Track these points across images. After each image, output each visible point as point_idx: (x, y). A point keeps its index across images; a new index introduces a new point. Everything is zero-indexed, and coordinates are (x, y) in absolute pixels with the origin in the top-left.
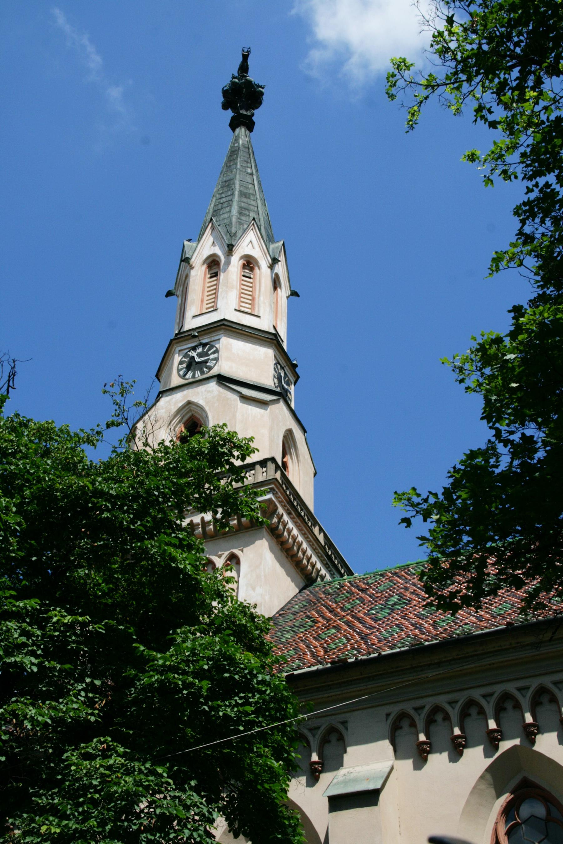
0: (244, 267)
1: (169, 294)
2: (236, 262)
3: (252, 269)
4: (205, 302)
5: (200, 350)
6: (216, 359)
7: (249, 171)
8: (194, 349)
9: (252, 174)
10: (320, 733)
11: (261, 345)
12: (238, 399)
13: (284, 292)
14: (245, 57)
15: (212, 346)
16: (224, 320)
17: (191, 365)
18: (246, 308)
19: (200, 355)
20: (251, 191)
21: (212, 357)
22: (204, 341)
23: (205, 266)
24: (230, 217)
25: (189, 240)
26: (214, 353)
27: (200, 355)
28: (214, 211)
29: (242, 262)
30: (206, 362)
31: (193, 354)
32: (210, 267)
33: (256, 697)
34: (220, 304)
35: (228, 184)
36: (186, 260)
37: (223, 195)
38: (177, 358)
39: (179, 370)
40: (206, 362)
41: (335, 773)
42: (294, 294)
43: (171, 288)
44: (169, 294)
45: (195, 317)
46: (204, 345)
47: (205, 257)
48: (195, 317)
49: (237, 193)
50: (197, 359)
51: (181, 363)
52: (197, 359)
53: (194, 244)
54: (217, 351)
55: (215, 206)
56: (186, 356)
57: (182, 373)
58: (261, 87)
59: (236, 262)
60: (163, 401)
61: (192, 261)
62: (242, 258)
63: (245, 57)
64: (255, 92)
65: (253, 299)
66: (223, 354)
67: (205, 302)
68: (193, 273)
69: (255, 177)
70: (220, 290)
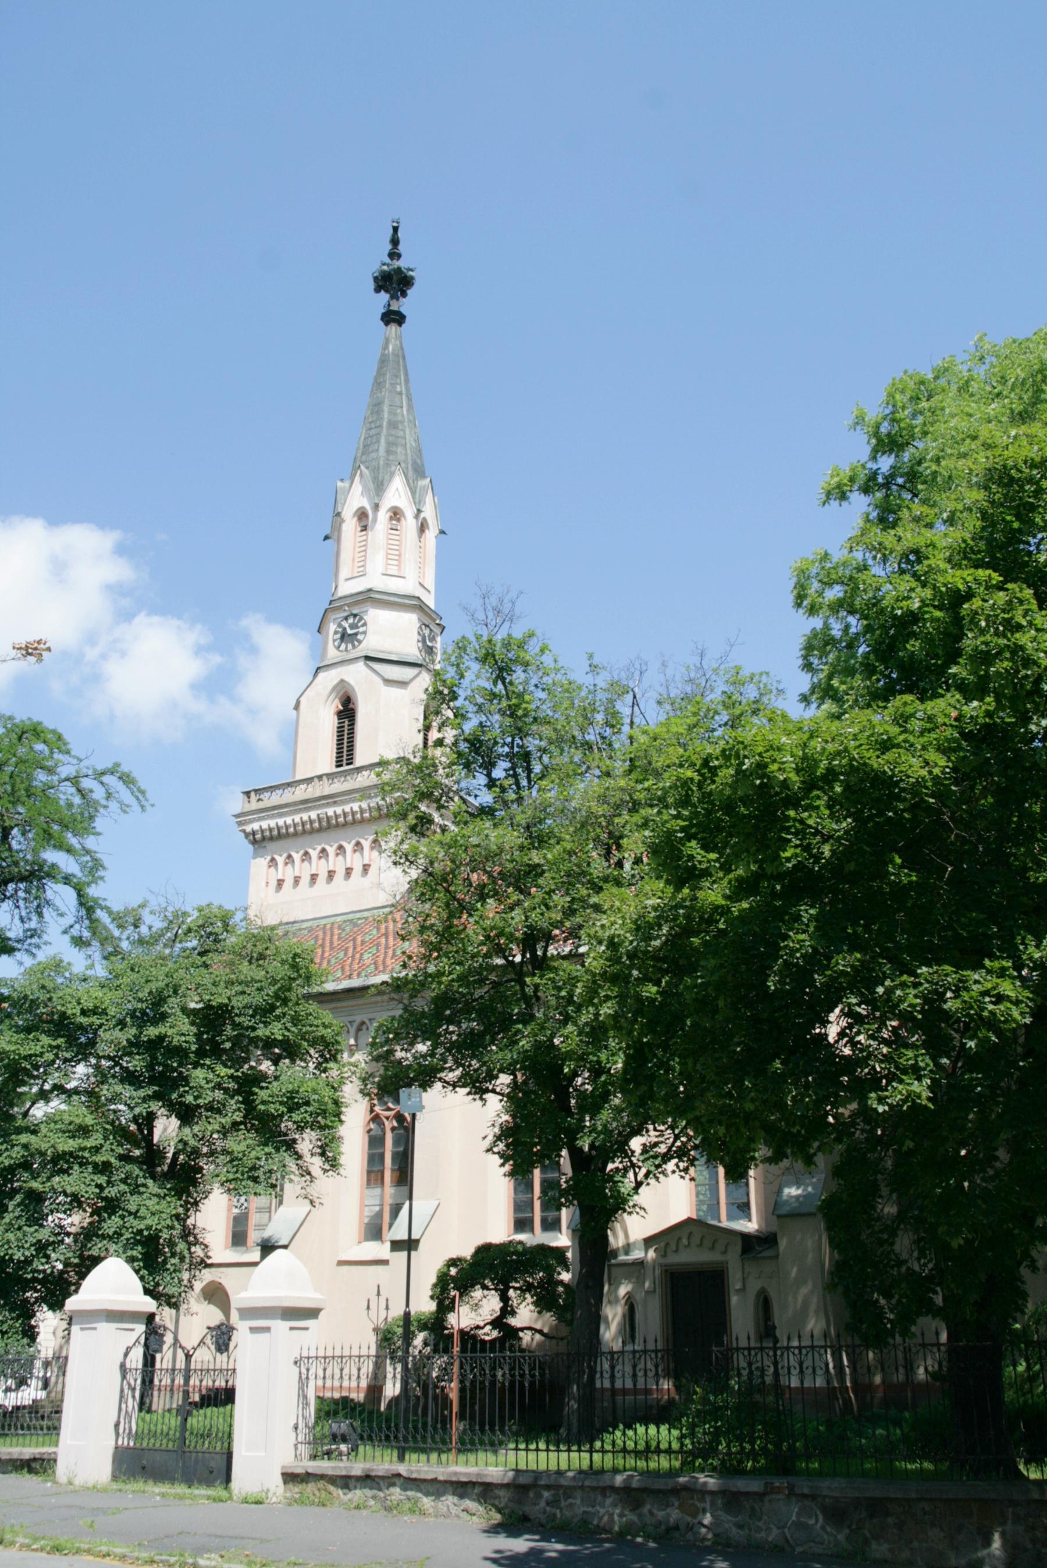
0: (391, 518)
1: (326, 538)
2: (383, 515)
3: (399, 520)
4: (357, 560)
5: (351, 620)
6: (365, 633)
7: (398, 389)
8: (346, 618)
9: (400, 393)
10: (355, 1025)
11: (405, 611)
12: (381, 682)
13: (431, 534)
14: (395, 229)
15: (361, 619)
16: (370, 590)
17: (344, 637)
18: (393, 570)
19: (352, 627)
20: (399, 418)
21: (361, 630)
22: (355, 612)
23: (356, 519)
24: (378, 458)
25: (342, 480)
26: (363, 625)
27: (352, 627)
28: (364, 446)
29: (390, 514)
30: (356, 634)
31: (345, 624)
32: (360, 519)
33: (427, 811)
34: (369, 568)
35: (376, 407)
36: (338, 514)
37: (373, 425)
38: (333, 627)
39: (334, 641)
40: (356, 634)
41: (546, 1243)
42: (442, 532)
43: (328, 532)
44: (326, 538)
45: (347, 580)
46: (355, 616)
47: (355, 510)
48: (347, 580)
49: (385, 424)
50: (349, 631)
51: (336, 633)
52: (349, 631)
53: (347, 484)
54: (365, 624)
55: (365, 439)
56: (340, 625)
57: (336, 643)
58: (412, 270)
59: (383, 515)
60: (322, 675)
61: (343, 515)
62: (389, 510)
63: (395, 229)
64: (406, 277)
65: (399, 555)
66: (370, 628)
67: (357, 560)
68: (344, 527)
69: (404, 397)
70: (368, 552)
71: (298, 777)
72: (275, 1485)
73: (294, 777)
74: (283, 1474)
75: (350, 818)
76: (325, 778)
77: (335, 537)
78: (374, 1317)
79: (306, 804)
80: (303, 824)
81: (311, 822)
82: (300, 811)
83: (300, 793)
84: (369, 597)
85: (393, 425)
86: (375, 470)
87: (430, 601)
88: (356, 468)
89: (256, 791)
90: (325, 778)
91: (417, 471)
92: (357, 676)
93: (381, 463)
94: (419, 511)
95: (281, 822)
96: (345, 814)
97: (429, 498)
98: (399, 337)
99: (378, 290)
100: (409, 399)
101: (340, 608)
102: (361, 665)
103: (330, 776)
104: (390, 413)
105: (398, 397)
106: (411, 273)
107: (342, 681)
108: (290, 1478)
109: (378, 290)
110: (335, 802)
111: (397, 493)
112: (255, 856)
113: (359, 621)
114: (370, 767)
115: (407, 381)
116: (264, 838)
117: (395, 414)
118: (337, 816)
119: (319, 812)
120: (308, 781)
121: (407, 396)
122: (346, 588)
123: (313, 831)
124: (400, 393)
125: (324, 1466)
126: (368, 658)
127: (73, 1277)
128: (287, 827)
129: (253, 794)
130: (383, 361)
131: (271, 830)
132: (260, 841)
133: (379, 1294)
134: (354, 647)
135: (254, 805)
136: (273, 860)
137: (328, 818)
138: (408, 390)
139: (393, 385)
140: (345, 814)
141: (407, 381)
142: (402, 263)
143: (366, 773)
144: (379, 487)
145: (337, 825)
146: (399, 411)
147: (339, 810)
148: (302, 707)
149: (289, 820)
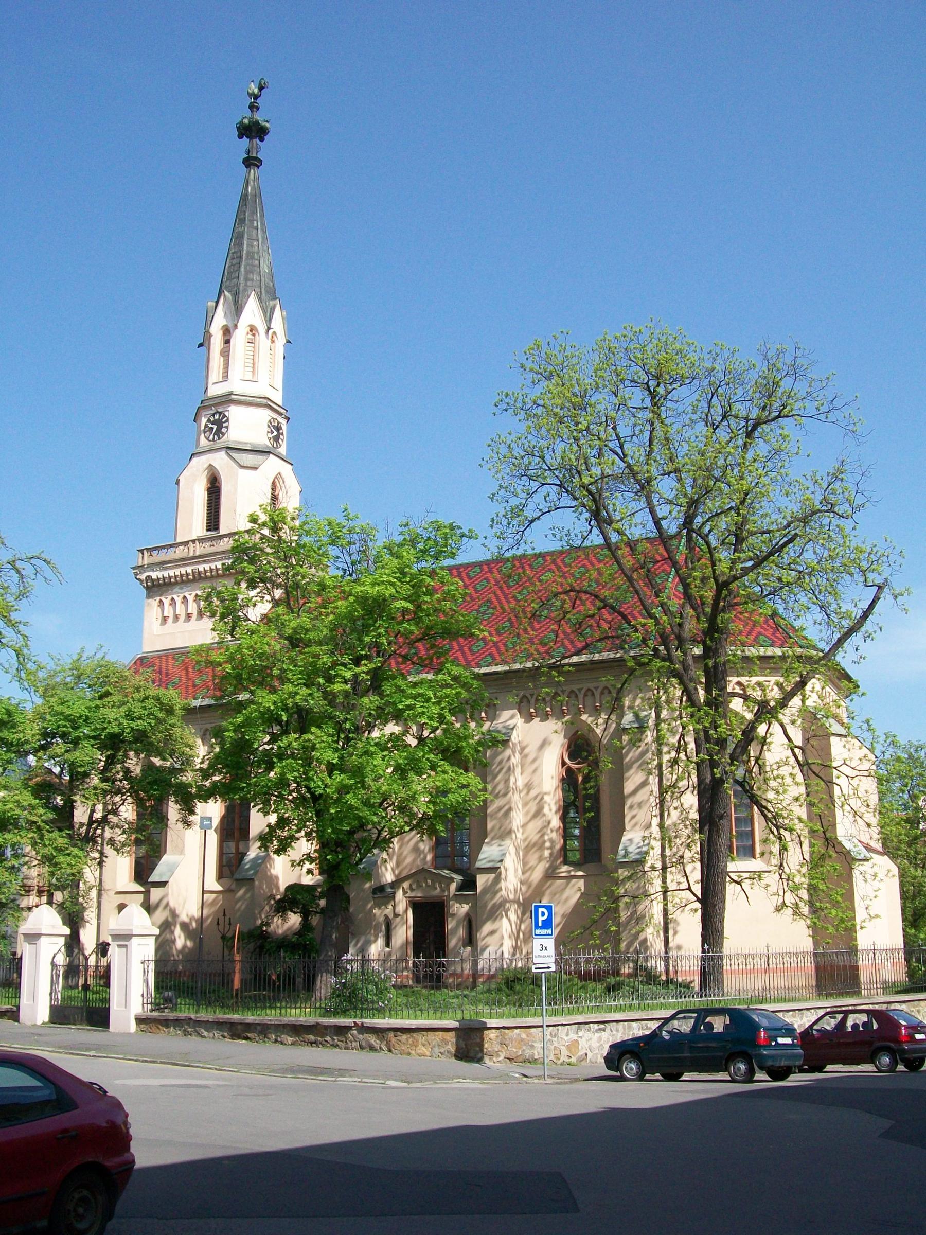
1: (201, 345)
32: (224, 334)
42: (288, 342)
44: (201, 345)
46: (220, 413)
60: (195, 460)
65: (254, 364)
71: (178, 541)
72: (133, 1027)
73: (175, 540)
74: (136, 1019)
75: (214, 573)
76: (197, 542)
77: (206, 344)
78: (222, 930)
79: (184, 561)
80: (182, 576)
81: (187, 575)
82: (180, 566)
83: (180, 552)
84: (228, 399)
85: (251, 256)
86: (236, 295)
87: (278, 397)
88: (220, 293)
89: (147, 549)
90: (197, 542)
91: (269, 296)
92: (220, 460)
93: (241, 288)
94: (269, 328)
95: (166, 574)
96: (211, 570)
97: (277, 313)
98: (256, 179)
99: (240, 137)
100: (264, 232)
101: (209, 407)
102: (223, 454)
103: (201, 540)
104: (248, 245)
105: (254, 231)
106: (268, 125)
107: (210, 465)
108: (140, 1021)
109: (240, 137)
110: (204, 561)
111: (252, 311)
112: (148, 597)
113: (223, 418)
114: (230, 535)
115: (262, 216)
116: (154, 586)
117: (252, 246)
118: (205, 571)
119: (193, 567)
120: (186, 543)
121: (262, 230)
122: (215, 390)
123: (189, 581)
124: (257, 228)
125: (168, 1014)
126: (228, 448)
127: (259, 1028)
128: (170, 578)
129: (145, 552)
130: (244, 198)
131: (158, 579)
132: (155, 588)
133: (224, 915)
134: (219, 438)
135: (147, 561)
136: (161, 601)
137: (199, 573)
138: (263, 224)
139: (252, 221)
140: (211, 570)
141: (262, 216)
142: (259, 117)
143: (226, 540)
144: (237, 309)
145: (206, 577)
146: (255, 243)
147: (207, 567)
148: (181, 483)
149: (172, 573)
